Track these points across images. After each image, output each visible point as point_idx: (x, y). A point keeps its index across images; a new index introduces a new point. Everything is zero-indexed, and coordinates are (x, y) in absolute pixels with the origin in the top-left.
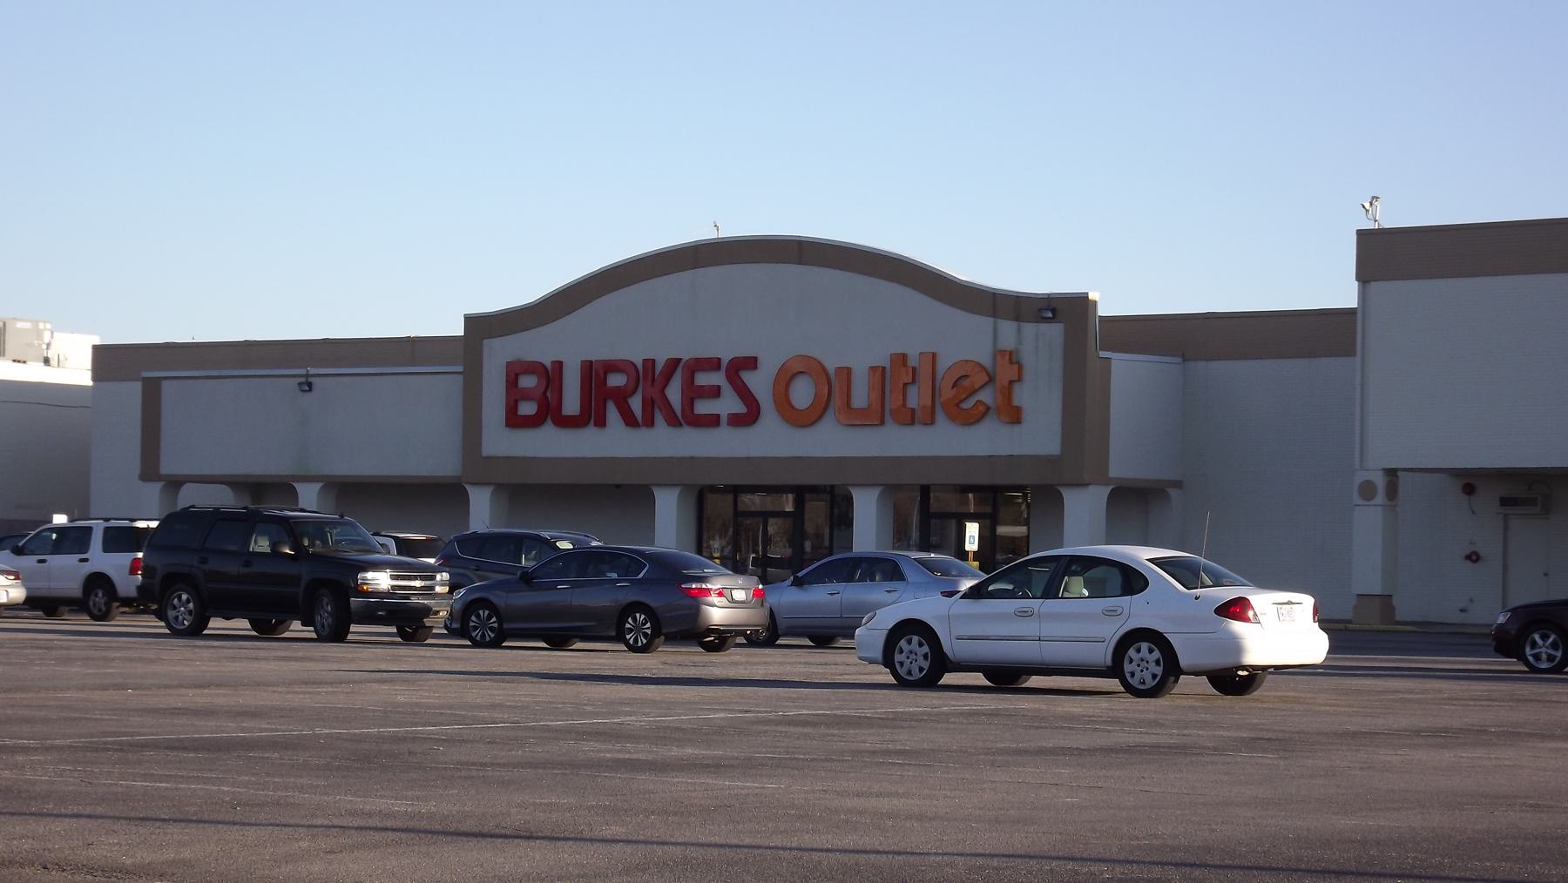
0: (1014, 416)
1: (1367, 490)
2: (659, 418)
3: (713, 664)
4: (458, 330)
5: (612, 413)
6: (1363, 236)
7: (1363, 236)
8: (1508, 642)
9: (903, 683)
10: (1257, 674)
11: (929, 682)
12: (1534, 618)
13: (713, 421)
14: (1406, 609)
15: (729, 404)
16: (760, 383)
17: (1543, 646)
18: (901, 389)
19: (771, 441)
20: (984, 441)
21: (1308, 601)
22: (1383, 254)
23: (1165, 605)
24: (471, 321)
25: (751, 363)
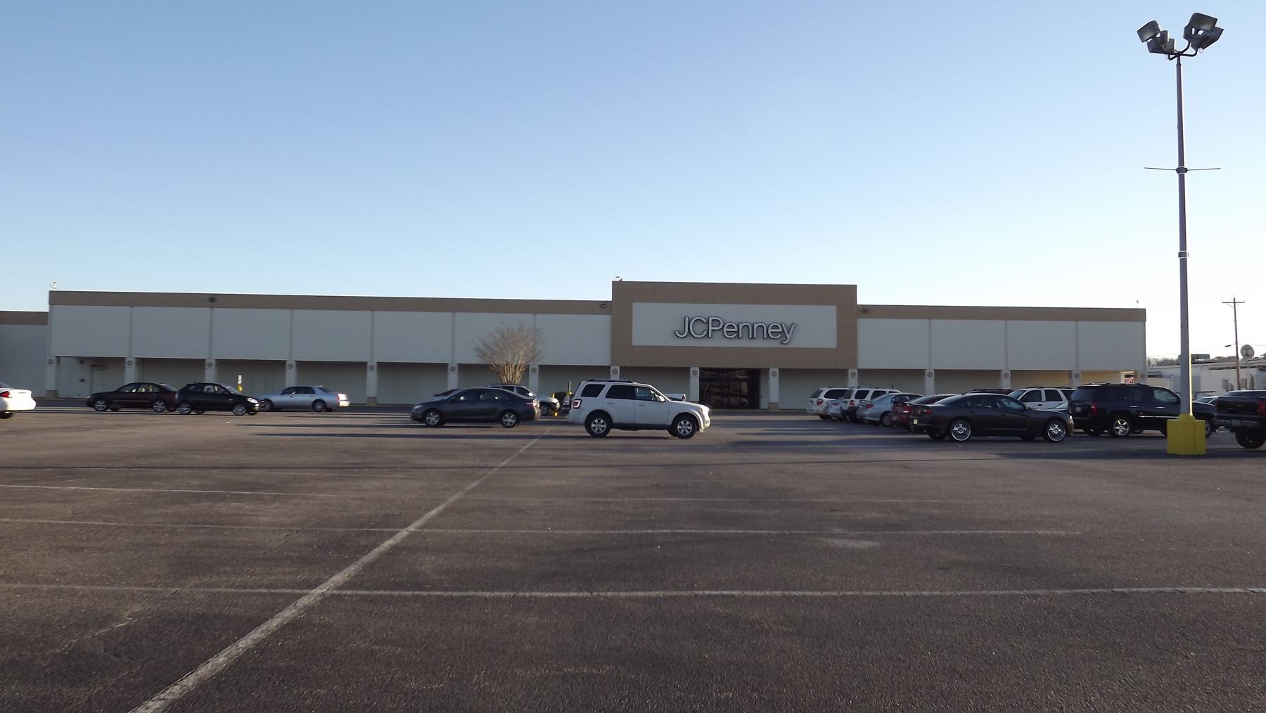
1: (50, 362)
4: (608, 297)
6: (51, 292)
7: (51, 292)
8: (90, 403)
9: (595, 436)
10: (12, 413)
11: (603, 436)
12: (99, 397)
14: (62, 394)
17: (100, 404)
21: (29, 393)
22: (57, 298)
23: (327, 398)
24: (619, 287)
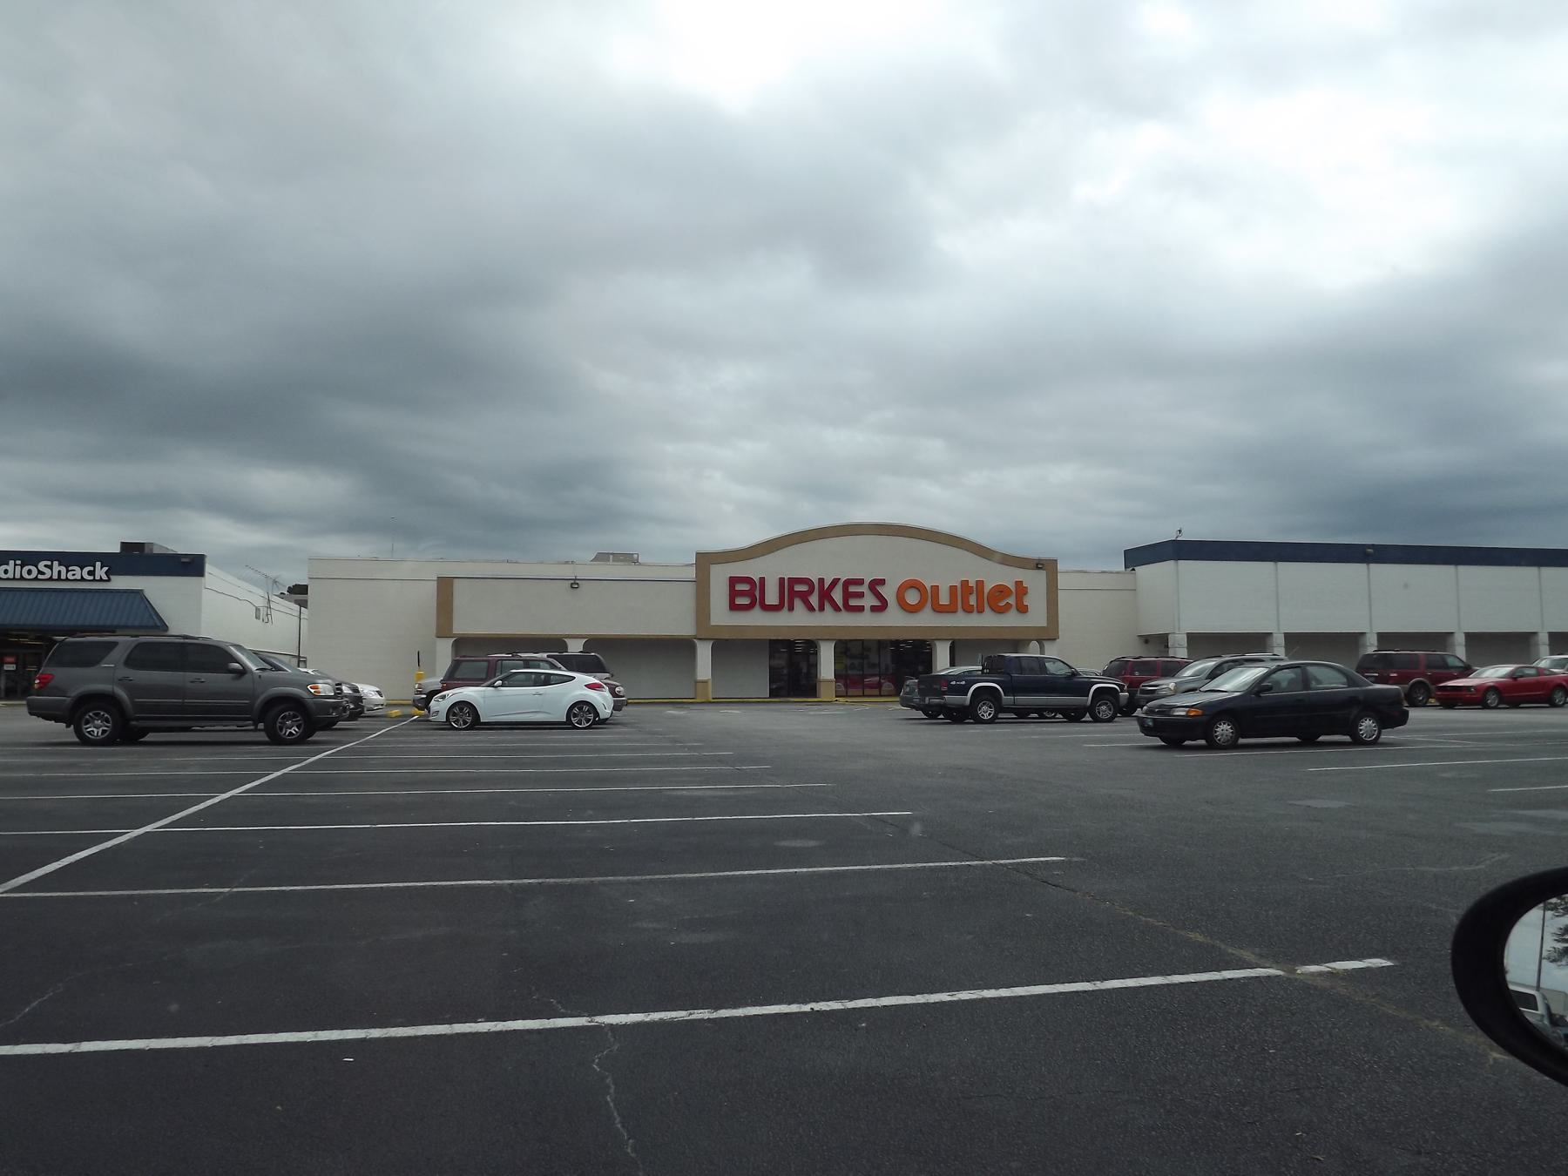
0: (1023, 609)
2: (827, 606)
3: (203, 766)
5: (798, 603)
13: (861, 609)
15: (869, 601)
16: (888, 592)
18: (966, 596)
19: (894, 620)
20: (1011, 620)
25: (882, 582)
